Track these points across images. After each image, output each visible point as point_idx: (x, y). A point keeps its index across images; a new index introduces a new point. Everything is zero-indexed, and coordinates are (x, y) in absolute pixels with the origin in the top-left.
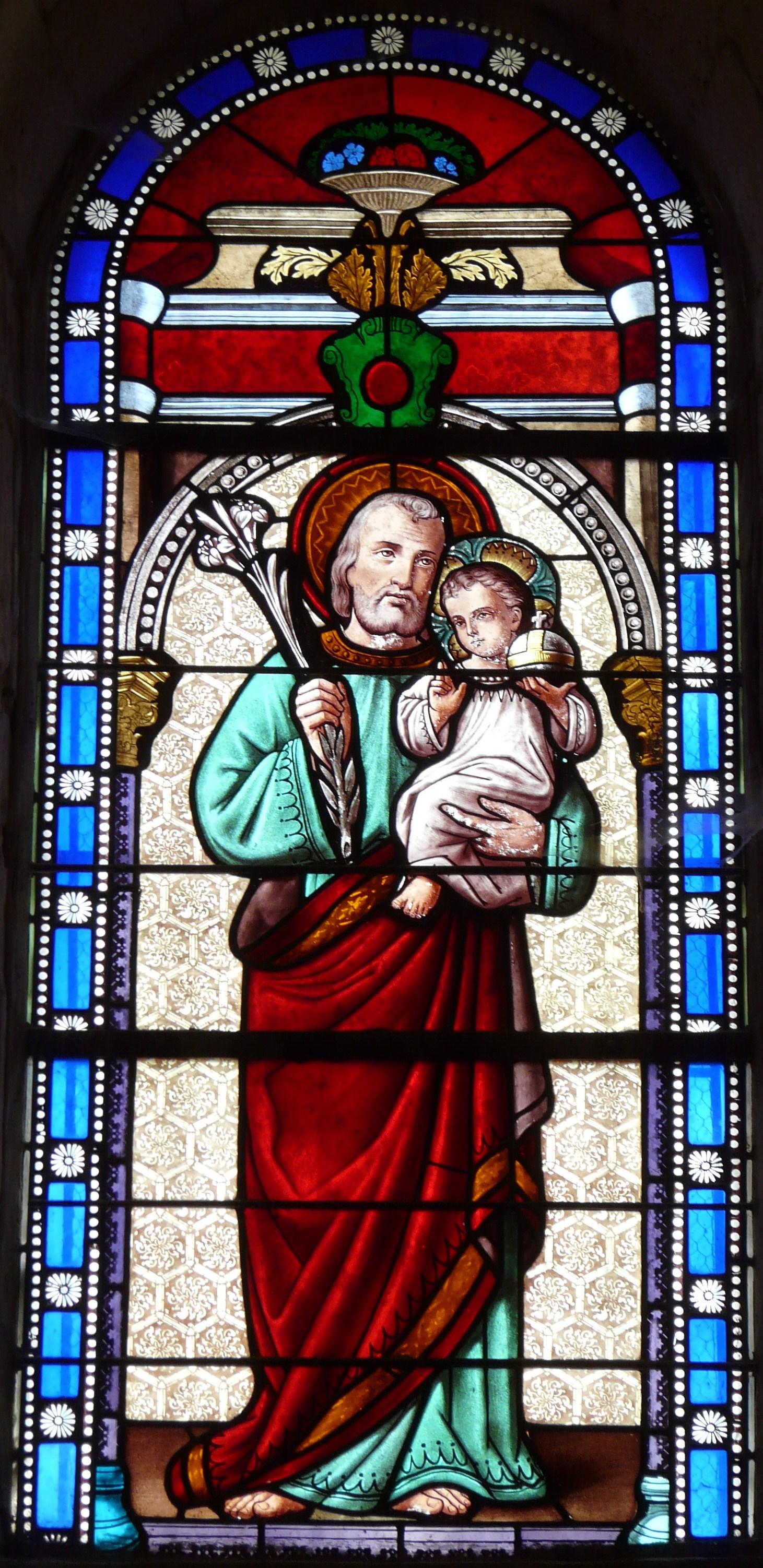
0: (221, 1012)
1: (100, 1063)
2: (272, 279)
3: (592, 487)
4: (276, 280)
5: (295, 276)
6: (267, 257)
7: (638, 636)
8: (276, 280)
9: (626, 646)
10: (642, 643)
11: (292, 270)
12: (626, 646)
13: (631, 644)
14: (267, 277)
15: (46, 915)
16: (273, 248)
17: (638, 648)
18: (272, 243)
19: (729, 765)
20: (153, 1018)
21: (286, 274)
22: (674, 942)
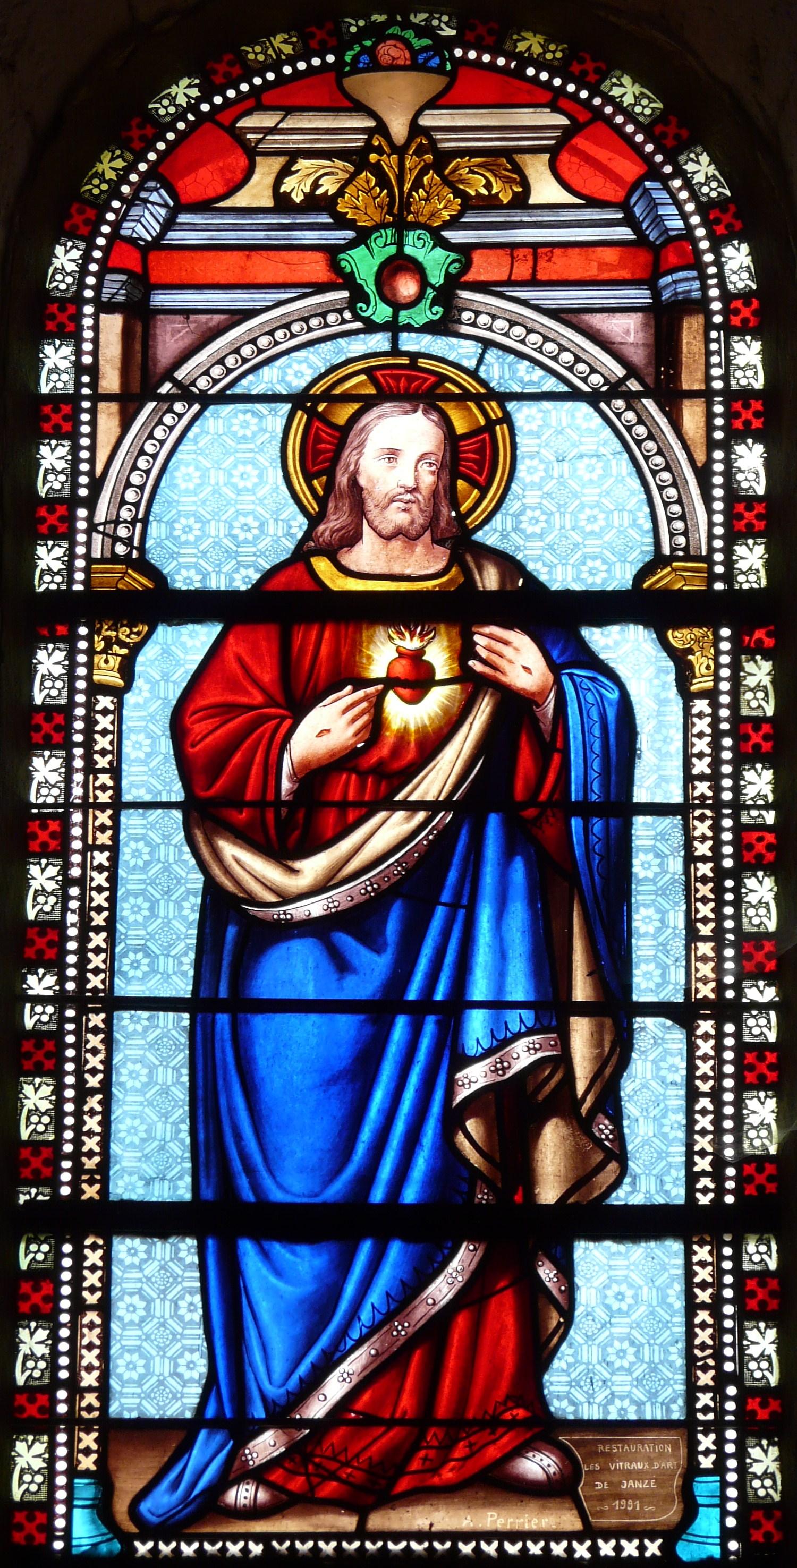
0: (641, 823)
1: (725, 632)
2: (293, 195)
3: (699, 297)
4: (298, 198)
5: (319, 192)
6: (286, 171)
7: (681, 540)
8: (298, 198)
9: (666, 551)
10: (686, 549)
11: (315, 185)
12: (666, 551)
13: (673, 549)
14: (287, 195)
15: (730, 1422)
16: (292, 162)
17: (681, 553)
18: (294, 156)
19: (70, 1027)
20: (674, 1407)
21: (307, 190)
22: (727, 850)
